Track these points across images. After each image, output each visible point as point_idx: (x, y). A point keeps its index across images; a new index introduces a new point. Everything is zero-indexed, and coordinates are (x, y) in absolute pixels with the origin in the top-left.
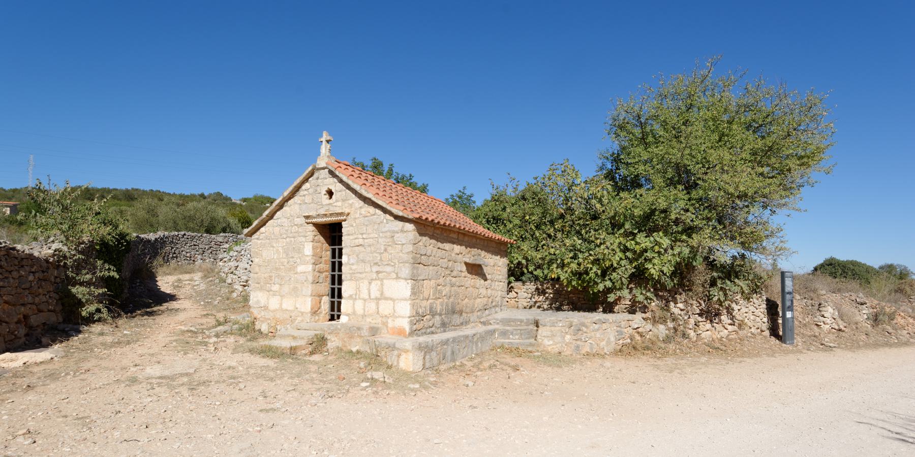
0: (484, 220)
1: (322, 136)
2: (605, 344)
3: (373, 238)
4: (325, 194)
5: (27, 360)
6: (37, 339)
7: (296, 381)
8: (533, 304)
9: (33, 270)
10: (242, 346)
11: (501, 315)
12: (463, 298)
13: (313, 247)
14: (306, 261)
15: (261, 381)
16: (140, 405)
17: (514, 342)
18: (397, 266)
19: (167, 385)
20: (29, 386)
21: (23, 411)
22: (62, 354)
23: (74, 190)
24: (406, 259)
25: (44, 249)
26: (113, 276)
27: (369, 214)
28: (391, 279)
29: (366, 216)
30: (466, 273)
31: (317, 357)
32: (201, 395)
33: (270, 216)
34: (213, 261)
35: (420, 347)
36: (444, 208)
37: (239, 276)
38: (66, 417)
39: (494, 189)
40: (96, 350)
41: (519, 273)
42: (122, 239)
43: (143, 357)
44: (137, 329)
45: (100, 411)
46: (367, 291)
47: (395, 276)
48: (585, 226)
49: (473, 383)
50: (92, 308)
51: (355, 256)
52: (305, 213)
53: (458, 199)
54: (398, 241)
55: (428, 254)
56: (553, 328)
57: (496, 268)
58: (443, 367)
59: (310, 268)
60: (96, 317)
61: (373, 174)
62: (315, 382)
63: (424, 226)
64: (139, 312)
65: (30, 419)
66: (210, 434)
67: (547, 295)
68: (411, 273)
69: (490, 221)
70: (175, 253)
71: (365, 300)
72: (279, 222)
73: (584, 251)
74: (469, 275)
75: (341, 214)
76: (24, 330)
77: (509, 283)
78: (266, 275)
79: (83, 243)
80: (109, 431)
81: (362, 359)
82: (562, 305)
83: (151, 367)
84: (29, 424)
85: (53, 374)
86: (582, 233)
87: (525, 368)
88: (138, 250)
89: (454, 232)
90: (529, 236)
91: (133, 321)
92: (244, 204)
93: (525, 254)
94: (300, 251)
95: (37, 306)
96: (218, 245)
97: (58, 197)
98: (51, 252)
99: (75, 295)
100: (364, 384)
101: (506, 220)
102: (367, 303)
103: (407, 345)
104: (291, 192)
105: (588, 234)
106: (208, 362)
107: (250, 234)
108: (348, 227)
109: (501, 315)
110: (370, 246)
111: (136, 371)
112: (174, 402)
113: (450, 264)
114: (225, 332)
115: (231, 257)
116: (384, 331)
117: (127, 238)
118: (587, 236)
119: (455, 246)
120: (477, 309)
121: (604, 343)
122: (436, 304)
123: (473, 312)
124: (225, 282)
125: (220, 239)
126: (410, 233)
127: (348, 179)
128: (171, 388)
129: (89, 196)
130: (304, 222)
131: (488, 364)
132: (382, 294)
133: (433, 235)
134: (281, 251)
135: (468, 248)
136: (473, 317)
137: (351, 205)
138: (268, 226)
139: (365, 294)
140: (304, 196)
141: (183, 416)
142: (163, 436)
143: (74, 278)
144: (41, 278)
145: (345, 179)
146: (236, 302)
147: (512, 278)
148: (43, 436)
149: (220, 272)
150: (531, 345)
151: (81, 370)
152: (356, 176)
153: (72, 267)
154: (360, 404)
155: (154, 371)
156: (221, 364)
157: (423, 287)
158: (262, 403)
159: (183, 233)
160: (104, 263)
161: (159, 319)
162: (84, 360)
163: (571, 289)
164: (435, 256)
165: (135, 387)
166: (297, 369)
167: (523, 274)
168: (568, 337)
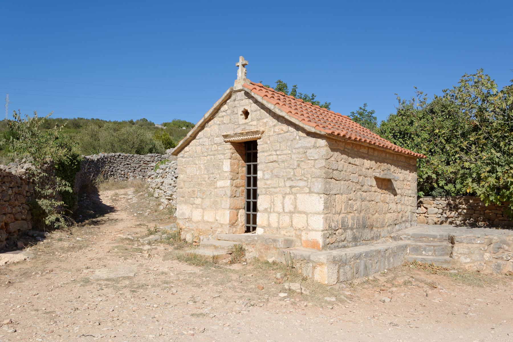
0: (391, 135)
1: (238, 61)
3: (286, 154)
4: (241, 115)
5: (7, 260)
6: (14, 243)
7: (220, 288)
8: (444, 219)
9: (11, 186)
10: (170, 253)
11: (412, 230)
12: (373, 213)
13: (230, 164)
15: (190, 286)
16: (93, 304)
17: (428, 258)
18: (309, 181)
19: (113, 286)
20: (10, 282)
21: (6, 303)
22: (32, 256)
23: (40, 119)
25: (19, 168)
26: (68, 190)
27: (282, 132)
29: (280, 134)
30: (376, 188)
31: (236, 267)
32: (141, 297)
33: (193, 136)
34: (142, 178)
35: (334, 261)
36: (351, 124)
37: (165, 191)
38: (37, 310)
39: (401, 103)
40: (57, 253)
41: (428, 188)
42: (74, 159)
43: (93, 261)
44: (86, 236)
45: (63, 307)
46: (281, 205)
47: (308, 191)
48: (504, 138)
49: (389, 300)
50: (53, 218)
51: (269, 171)
52: (224, 133)
53: (359, 116)
55: (339, 169)
56: (470, 245)
57: (405, 182)
58: (356, 281)
59: (228, 183)
60: (56, 225)
61: (284, 94)
62: (237, 290)
63: (336, 142)
64: (87, 221)
65: (11, 310)
66: (151, 334)
67: (460, 211)
68: (323, 188)
69: (397, 136)
70: (112, 171)
71: (279, 214)
73: (503, 164)
74: (379, 190)
75: (257, 132)
76: (5, 235)
77: (419, 197)
78: (190, 190)
79: (46, 163)
80: (70, 325)
81: (278, 270)
82: (476, 221)
83: (99, 270)
84: (11, 315)
85: (26, 273)
86: (501, 145)
87: (442, 286)
88: (85, 169)
89: (364, 147)
90: (439, 150)
91: (83, 229)
92: (165, 128)
93: (435, 168)
94: (219, 167)
95: (14, 215)
96: (146, 164)
97: (29, 125)
98: (23, 170)
99: (41, 207)
100: (282, 295)
101: (413, 134)
102: (281, 216)
103: (322, 258)
104: (211, 114)
105: (508, 146)
106: (144, 267)
107: (176, 153)
108: (262, 144)
109: (412, 230)
110: (283, 162)
111: (88, 273)
112: (120, 303)
113: (361, 178)
114: (156, 241)
115: (158, 174)
116: (298, 243)
117: (78, 159)
118: (506, 148)
119: (365, 160)
120: (387, 224)
122: (347, 218)
123: (383, 227)
124: (153, 196)
125: (148, 159)
126: (322, 148)
127: (262, 99)
128: (116, 289)
129: (47, 125)
130: (223, 141)
131: (402, 280)
132: (295, 207)
133: (344, 150)
134: (203, 168)
135: (378, 163)
136: (384, 232)
137: (265, 124)
138: (191, 146)
139: (279, 208)
140: (223, 117)
141: (128, 316)
142: (113, 333)
143: (40, 192)
144: (17, 192)
145: (259, 99)
146: (163, 214)
147: (421, 193)
148: (21, 326)
149: (149, 187)
150: (446, 262)
151: (47, 270)
152: (270, 96)
153: (38, 183)
154: (280, 314)
155: (102, 273)
156: (155, 269)
157: (335, 201)
158: (192, 308)
159: (118, 154)
160: (62, 180)
161: (103, 228)
162: (48, 261)
164: (346, 171)
165: (88, 288)
166: (220, 277)
167: (432, 189)
168: (487, 256)
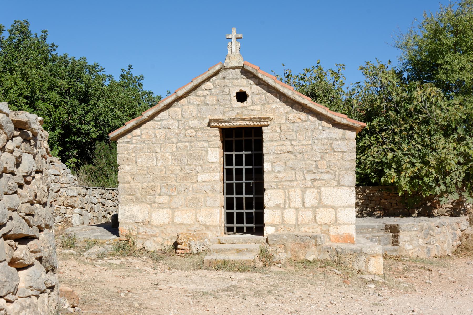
1: (231, 33)
2: (446, 246)
4: (235, 96)
14: (212, 169)
18: (337, 173)
24: (348, 167)
28: (331, 186)
46: (300, 200)
47: (335, 184)
51: (281, 163)
54: (336, 148)
56: (410, 233)
71: (297, 209)
72: (163, 123)
75: (265, 119)
82: (373, 210)
102: (300, 212)
110: (301, 153)
121: (445, 246)
127: (275, 82)
134: (170, 157)
137: (274, 110)
140: (204, 96)
163: (402, 194)
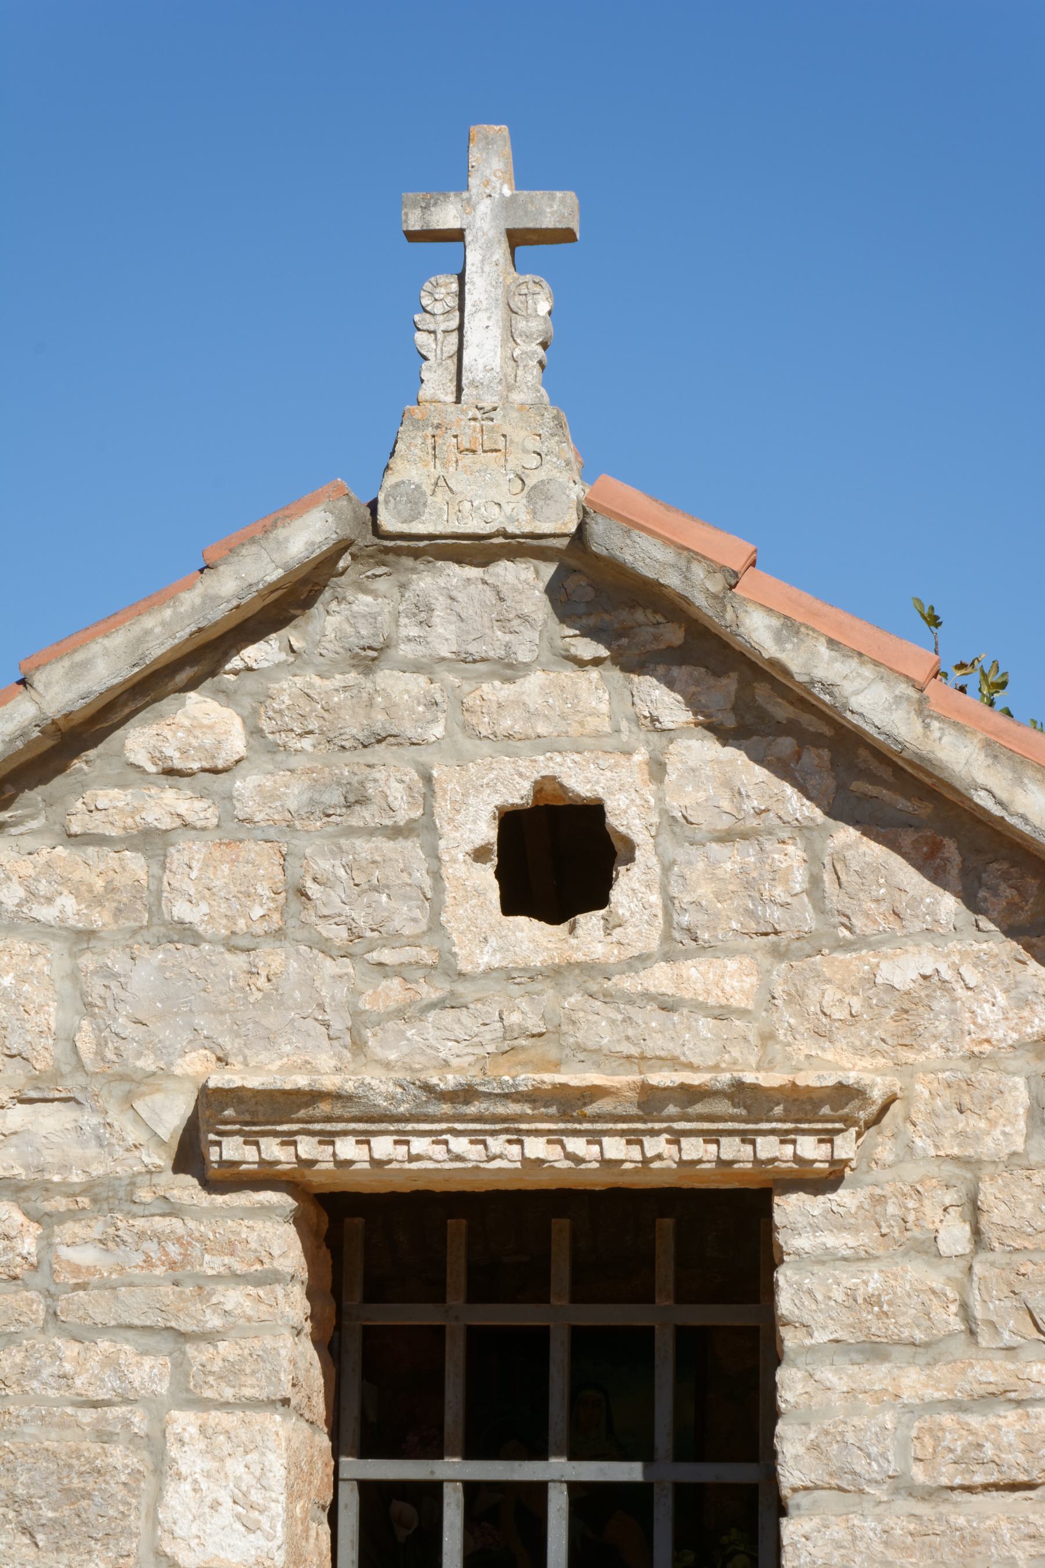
108: (861, 1258)
127: (922, 709)
